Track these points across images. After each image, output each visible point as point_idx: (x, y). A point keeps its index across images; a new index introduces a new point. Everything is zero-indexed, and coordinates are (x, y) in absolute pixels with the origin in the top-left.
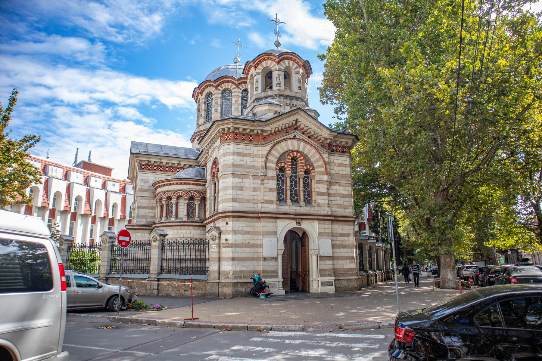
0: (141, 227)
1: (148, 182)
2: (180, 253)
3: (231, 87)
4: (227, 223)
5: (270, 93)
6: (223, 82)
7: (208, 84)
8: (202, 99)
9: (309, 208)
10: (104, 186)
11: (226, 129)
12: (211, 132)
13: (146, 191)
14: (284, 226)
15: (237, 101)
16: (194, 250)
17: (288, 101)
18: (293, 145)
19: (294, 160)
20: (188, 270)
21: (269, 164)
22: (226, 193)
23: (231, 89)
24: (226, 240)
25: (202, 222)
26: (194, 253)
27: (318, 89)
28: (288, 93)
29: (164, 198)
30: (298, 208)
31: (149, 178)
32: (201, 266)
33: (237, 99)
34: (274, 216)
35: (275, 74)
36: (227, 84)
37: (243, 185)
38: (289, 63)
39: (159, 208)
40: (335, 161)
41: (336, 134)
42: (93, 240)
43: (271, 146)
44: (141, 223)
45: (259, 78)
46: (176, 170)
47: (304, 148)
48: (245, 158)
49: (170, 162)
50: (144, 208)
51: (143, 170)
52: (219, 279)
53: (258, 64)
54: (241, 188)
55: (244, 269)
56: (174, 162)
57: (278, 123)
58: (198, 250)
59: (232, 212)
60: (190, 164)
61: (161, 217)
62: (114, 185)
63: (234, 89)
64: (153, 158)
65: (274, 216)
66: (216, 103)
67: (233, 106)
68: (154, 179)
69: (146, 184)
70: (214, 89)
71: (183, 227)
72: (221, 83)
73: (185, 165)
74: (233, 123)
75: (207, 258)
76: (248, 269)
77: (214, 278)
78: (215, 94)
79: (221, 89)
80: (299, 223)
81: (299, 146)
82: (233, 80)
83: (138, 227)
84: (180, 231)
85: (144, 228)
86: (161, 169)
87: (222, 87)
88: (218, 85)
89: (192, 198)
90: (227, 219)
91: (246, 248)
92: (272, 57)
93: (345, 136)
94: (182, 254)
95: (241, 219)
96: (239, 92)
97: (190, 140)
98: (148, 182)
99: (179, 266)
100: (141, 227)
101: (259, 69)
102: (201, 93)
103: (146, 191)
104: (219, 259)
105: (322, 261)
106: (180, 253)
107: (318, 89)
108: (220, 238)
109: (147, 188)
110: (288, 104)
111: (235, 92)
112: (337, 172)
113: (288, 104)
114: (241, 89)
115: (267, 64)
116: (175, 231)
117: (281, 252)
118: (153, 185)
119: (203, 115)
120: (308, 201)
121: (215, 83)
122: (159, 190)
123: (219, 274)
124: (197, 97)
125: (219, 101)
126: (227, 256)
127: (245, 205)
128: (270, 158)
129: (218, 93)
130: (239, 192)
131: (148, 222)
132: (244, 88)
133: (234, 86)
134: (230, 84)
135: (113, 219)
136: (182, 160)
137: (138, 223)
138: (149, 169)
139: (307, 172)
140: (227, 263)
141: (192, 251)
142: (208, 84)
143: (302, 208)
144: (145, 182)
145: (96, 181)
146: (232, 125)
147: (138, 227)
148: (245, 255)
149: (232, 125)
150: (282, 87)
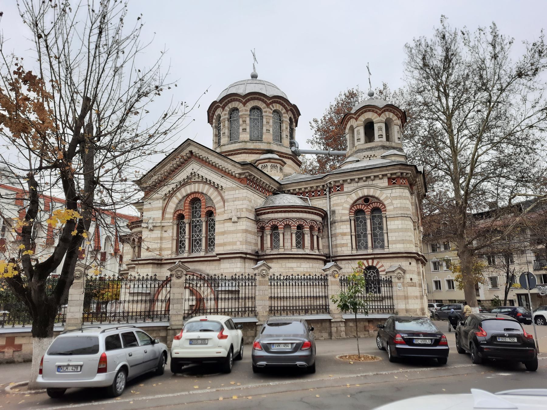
4: (410, 263)
8: (225, 114)
24: (411, 279)
27: (385, 86)
29: (294, 226)
35: (376, 127)
38: (389, 115)
45: (362, 130)
67: (241, 128)
72: (227, 104)
74: (400, 169)
82: (262, 98)
84: (315, 265)
87: (273, 107)
90: (410, 260)
96: (270, 112)
102: (223, 108)
106: (279, 290)
107: (385, 86)
111: (266, 112)
114: (272, 110)
116: (311, 264)
119: (226, 134)
133: (264, 105)
146: (399, 171)
149: (399, 171)
150: (384, 138)
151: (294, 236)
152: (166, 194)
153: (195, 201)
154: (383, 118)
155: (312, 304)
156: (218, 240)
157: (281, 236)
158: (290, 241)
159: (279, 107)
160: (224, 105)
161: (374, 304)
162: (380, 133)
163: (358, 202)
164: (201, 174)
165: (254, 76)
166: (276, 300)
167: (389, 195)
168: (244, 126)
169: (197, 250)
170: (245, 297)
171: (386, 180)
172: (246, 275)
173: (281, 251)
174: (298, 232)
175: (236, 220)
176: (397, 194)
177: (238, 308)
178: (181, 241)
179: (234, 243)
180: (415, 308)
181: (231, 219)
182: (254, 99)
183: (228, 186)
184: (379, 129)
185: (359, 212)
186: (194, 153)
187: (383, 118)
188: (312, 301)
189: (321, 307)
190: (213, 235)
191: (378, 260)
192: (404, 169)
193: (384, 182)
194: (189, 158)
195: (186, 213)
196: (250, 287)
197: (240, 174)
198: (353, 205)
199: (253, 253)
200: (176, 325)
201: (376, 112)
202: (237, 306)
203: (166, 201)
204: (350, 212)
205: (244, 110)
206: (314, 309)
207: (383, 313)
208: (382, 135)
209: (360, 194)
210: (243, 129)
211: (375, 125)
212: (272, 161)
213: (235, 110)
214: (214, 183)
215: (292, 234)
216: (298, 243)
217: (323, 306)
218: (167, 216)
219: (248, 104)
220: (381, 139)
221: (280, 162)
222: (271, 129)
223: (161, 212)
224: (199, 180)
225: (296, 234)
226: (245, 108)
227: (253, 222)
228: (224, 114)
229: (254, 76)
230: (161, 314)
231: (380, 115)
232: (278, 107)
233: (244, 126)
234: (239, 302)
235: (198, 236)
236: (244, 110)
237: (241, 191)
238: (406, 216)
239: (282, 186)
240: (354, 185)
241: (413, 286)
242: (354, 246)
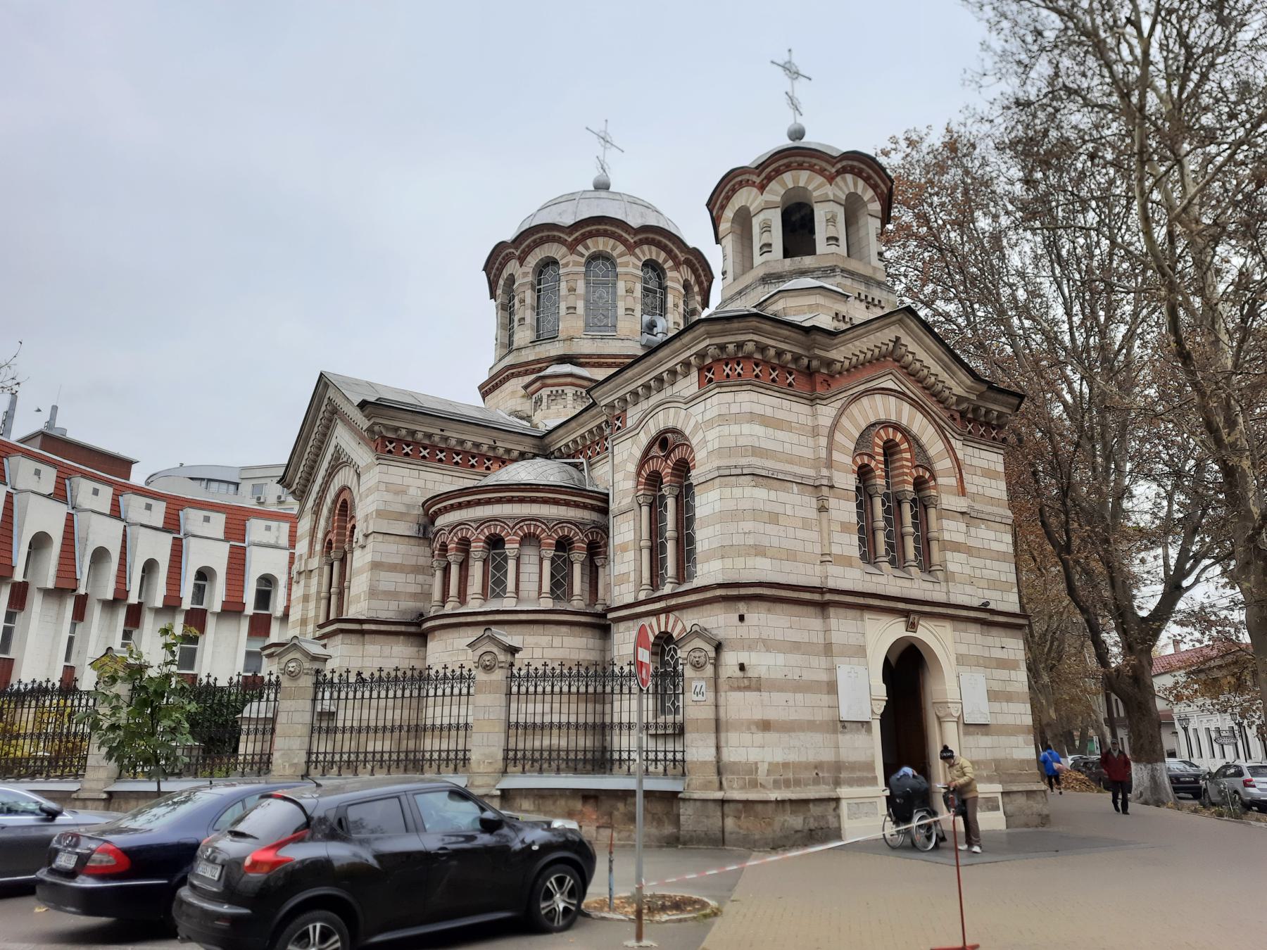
0: (383, 628)
1: (404, 492)
2: (531, 706)
3: (614, 248)
4: (742, 618)
5: (807, 262)
6: (591, 235)
7: (546, 233)
8: (525, 274)
9: (929, 586)
10: (116, 513)
11: (731, 347)
12: (661, 354)
13: (400, 516)
14: (884, 634)
15: (629, 291)
16: (573, 698)
17: (862, 288)
18: (887, 410)
19: (890, 449)
20: (533, 760)
21: (836, 456)
22: (733, 531)
23: (615, 254)
24: (742, 667)
25: (419, 625)
26: (573, 706)
28: (853, 265)
29: (478, 540)
30: (907, 583)
31: (407, 481)
32: (589, 744)
33: (630, 285)
34: (861, 601)
35: (820, 214)
36: (601, 240)
37: (778, 509)
39: (439, 574)
40: (975, 462)
41: (984, 388)
42: (72, 668)
43: (838, 404)
44: (383, 616)
46: (481, 464)
48: (780, 435)
49: (471, 437)
50: (393, 568)
51: (407, 459)
52: (721, 787)
53: (769, 179)
54: (774, 518)
55: (792, 757)
56: (480, 440)
57: (857, 343)
58: (585, 697)
59: (720, 586)
60: (521, 448)
61: (444, 600)
62: (149, 507)
63: (621, 255)
64: (422, 424)
65: (861, 601)
66: (572, 290)
67: (563, 306)
68: (420, 483)
69: (399, 499)
71: (541, 627)
72: (585, 237)
73: (508, 451)
74: (710, 335)
75: (616, 720)
76: (803, 759)
77: (706, 786)
78: (566, 265)
79: (587, 254)
80: (912, 626)
81: (899, 413)
83: (373, 627)
85: (393, 628)
86: (441, 456)
87: (587, 248)
88: (578, 241)
89: (563, 545)
90: (742, 607)
91: (795, 692)
92: (814, 161)
93: (1000, 397)
94: (531, 710)
95: (779, 607)
97: (480, 388)
98: (404, 492)
99: (529, 745)
100: (383, 628)
101: (774, 192)
102: (522, 260)
103: (400, 516)
104: (718, 726)
105: (971, 738)
106: (531, 706)
108: (716, 664)
109: (403, 509)
110: (863, 297)
111: (626, 265)
112: (981, 491)
113: (863, 297)
114: (582, 255)
115: (796, 180)
117: (880, 708)
118: (426, 505)
120: (926, 564)
121: (517, 248)
122: (441, 521)
123: (719, 773)
126: (746, 715)
127: (787, 566)
128: (838, 437)
129: (576, 264)
130: (770, 528)
131: (404, 612)
132: (648, 257)
134: (612, 242)
135: (140, 606)
136: (502, 435)
137: (372, 615)
138: (407, 454)
139: (919, 484)
140: (746, 737)
141: (565, 698)
142: (546, 233)
143: (916, 586)
144: (397, 493)
145: (96, 492)
146: (707, 342)
147: (373, 627)
148: (805, 715)
149: (707, 342)
150: (842, 249)
151: (547, 565)
154: (776, 192)
155: (521, 746)
157: (511, 565)
158: (536, 578)
161: (661, 748)
162: (766, 238)
165: (602, 186)
166: (547, 732)
167: (699, 418)
170: (385, 727)
172: (556, 666)
173: (509, 604)
174: (559, 557)
176: (746, 408)
177: (357, 753)
180: (752, 759)
182: (538, 244)
184: (827, 222)
185: (654, 480)
187: (776, 192)
188: (573, 738)
189: (554, 755)
191: (677, 613)
192: (723, 333)
193: (688, 385)
196: (399, 702)
199: (408, 618)
200: (91, 790)
201: (821, 172)
202: (329, 749)
204: (638, 483)
205: (571, 264)
207: (541, 771)
208: (837, 239)
212: (549, 381)
213: (551, 262)
215: (541, 560)
216: (556, 585)
217: (559, 751)
219: (529, 258)
220: (833, 249)
221: (569, 380)
222: (580, 305)
225: (553, 561)
226: (525, 269)
227: (412, 541)
229: (602, 186)
230: (665, 760)
236: (630, 266)
238: (734, 472)
239: (547, 441)
241: (748, 688)
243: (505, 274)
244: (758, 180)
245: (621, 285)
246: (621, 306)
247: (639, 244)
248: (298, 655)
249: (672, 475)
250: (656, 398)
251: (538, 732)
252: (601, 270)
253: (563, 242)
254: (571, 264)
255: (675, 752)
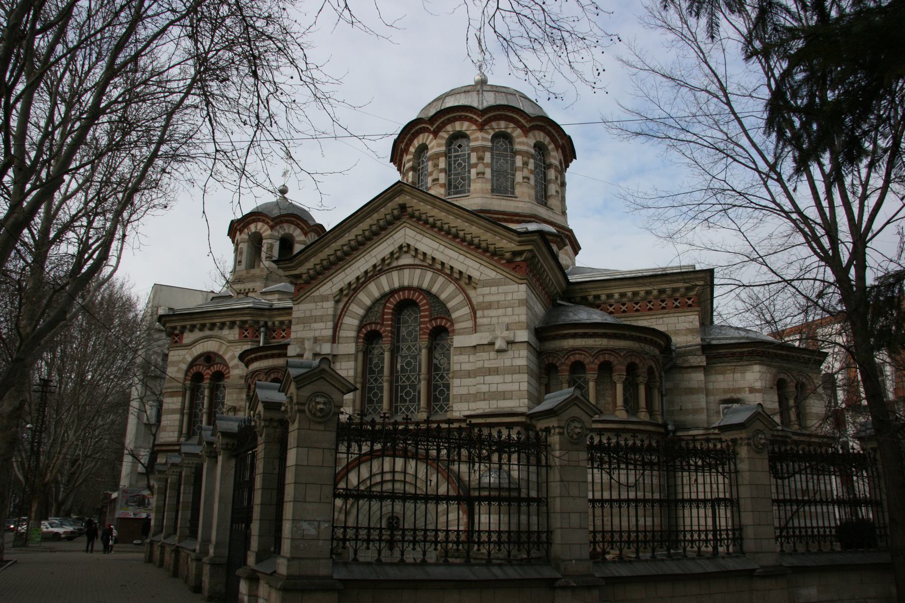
47: (433, 282)
53: (276, 224)
63: (518, 136)
67: (473, 171)
70: (431, 136)
72: (444, 124)
101: (442, 138)
102: (436, 134)
121: (432, 124)
124: (401, 160)
125: (442, 163)
129: (439, 145)
152: (341, 290)
153: (405, 303)
154: (279, 232)
156: (458, 387)
159: (544, 138)
160: (437, 127)
163: (198, 362)
164: (422, 248)
168: (480, 168)
169: (441, 408)
171: (236, 331)
175: (504, 346)
178: (371, 389)
179: (504, 395)
181: (492, 344)
183: (483, 277)
185: (197, 378)
186: (409, 210)
187: (279, 232)
190: (442, 377)
194: (397, 218)
195: (386, 329)
197: (515, 254)
198: (192, 365)
203: (341, 305)
206: (645, 542)
209: (198, 350)
210: (478, 174)
211: (264, 241)
213: (461, 135)
214: (452, 268)
217: (629, 532)
218: (343, 333)
222: (488, 171)
223: (330, 324)
224: (417, 262)
228: (436, 145)
231: (272, 228)
232: (541, 137)
233: (526, 173)
234: (637, 525)
235: (376, 380)
237: (515, 287)
240: (197, 334)
242: (184, 431)
243: (416, 143)
244: (271, 223)
245: (519, 161)
246: (519, 177)
247: (532, 128)
248: (327, 388)
249: (211, 379)
250: (207, 333)
251: (687, 505)
252: (502, 145)
253: (474, 122)
254: (479, 138)
255: (357, 539)
